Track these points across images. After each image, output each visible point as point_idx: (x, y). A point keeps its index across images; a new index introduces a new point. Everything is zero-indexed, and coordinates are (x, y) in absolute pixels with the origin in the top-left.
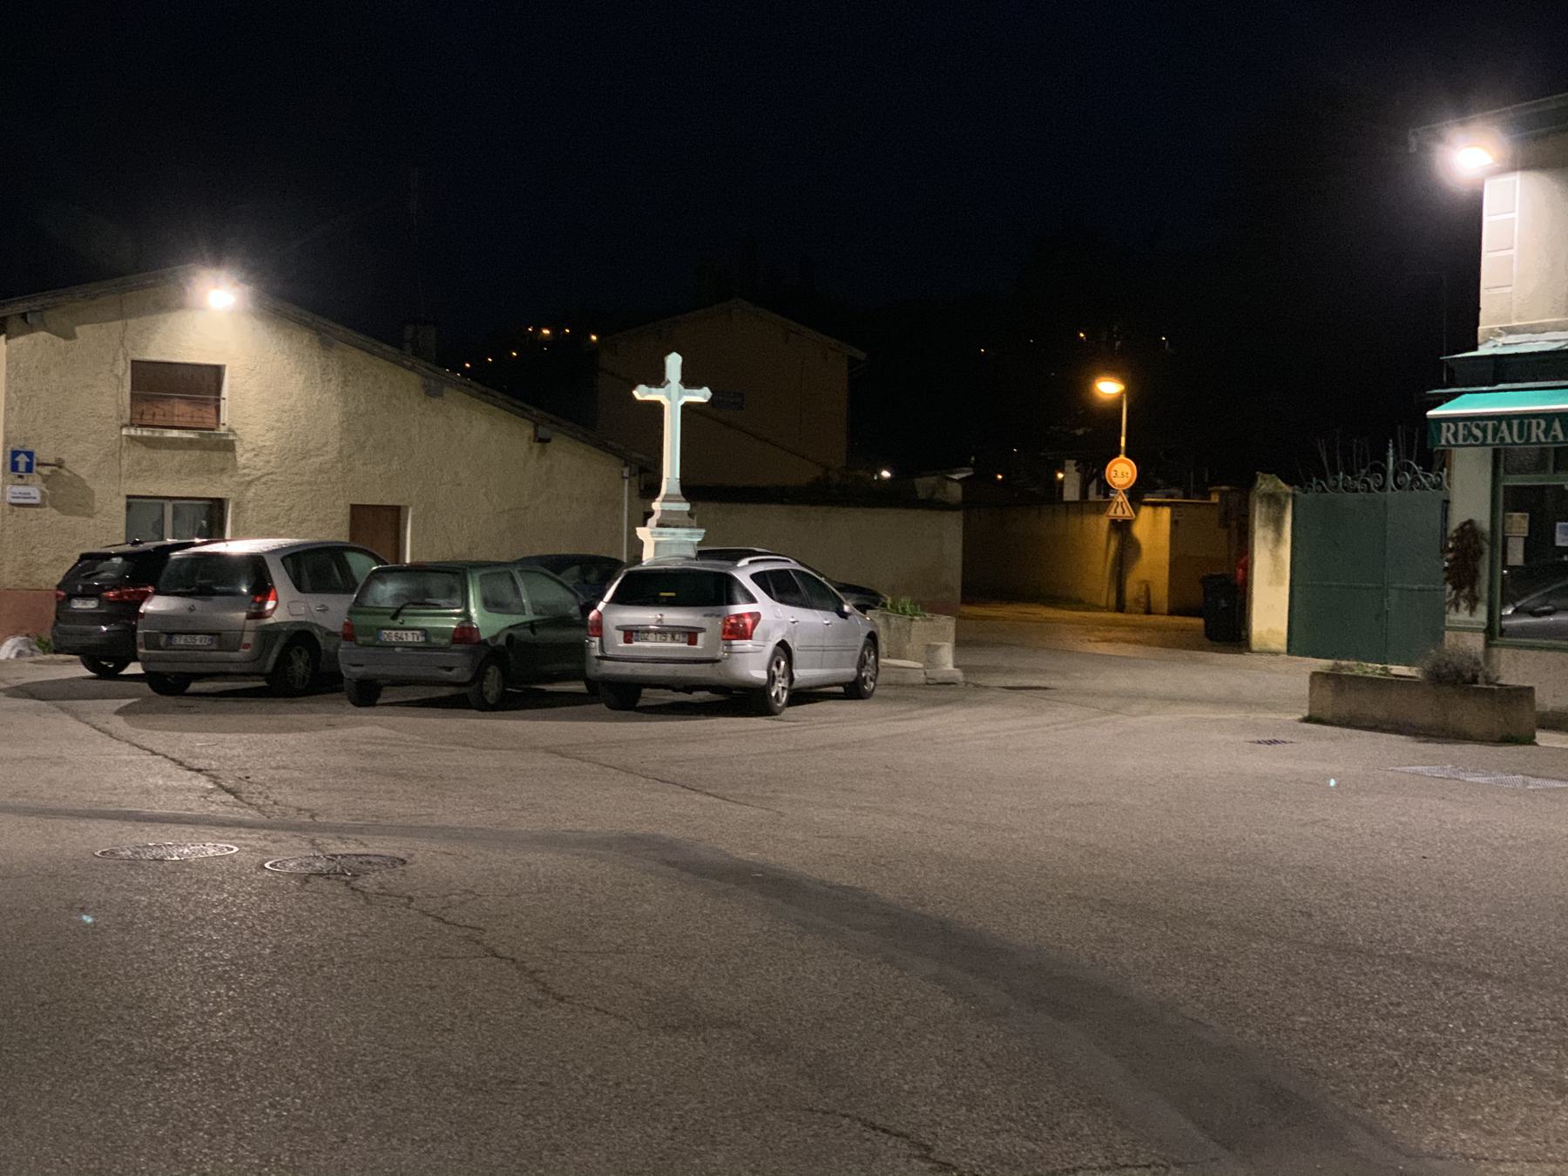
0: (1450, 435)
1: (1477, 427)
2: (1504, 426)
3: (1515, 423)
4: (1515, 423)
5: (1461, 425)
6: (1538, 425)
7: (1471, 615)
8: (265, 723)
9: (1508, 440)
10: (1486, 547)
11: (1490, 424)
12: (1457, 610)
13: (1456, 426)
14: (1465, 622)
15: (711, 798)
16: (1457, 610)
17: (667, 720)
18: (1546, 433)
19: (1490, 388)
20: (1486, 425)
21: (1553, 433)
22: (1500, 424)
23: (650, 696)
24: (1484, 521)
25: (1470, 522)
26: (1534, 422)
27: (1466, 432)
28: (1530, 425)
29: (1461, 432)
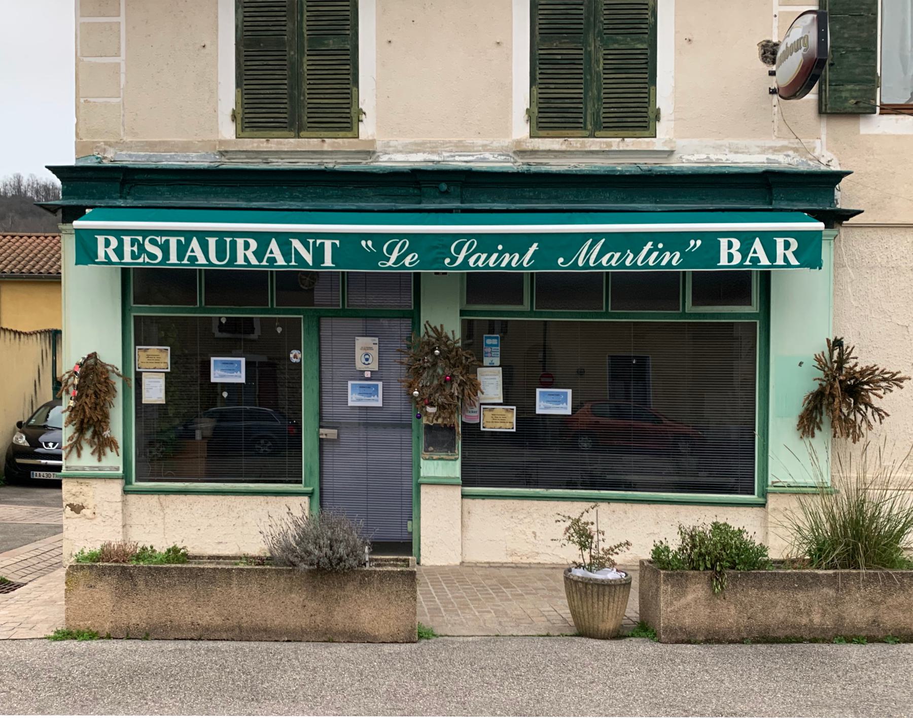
0: (110, 251)
1: (153, 242)
2: (195, 243)
3: (212, 242)
4: (212, 242)
5: (127, 240)
6: (247, 246)
7: (100, 460)
8: (202, 190)
9: (202, 260)
10: (119, 386)
11: (173, 241)
12: (79, 455)
13: (121, 243)
14: (92, 468)
15: (796, 208)
16: (79, 455)
17: (443, 230)
18: (259, 254)
19: (136, 203)
20: (167, 242)
21: (268, 255)
22: (188, 242)
23: (454, 211)
24: (111, 356)
25: (93, 356)
26: (240, 242)
27: (135, 249)
28: (234, 245)
29: (127, 249)
